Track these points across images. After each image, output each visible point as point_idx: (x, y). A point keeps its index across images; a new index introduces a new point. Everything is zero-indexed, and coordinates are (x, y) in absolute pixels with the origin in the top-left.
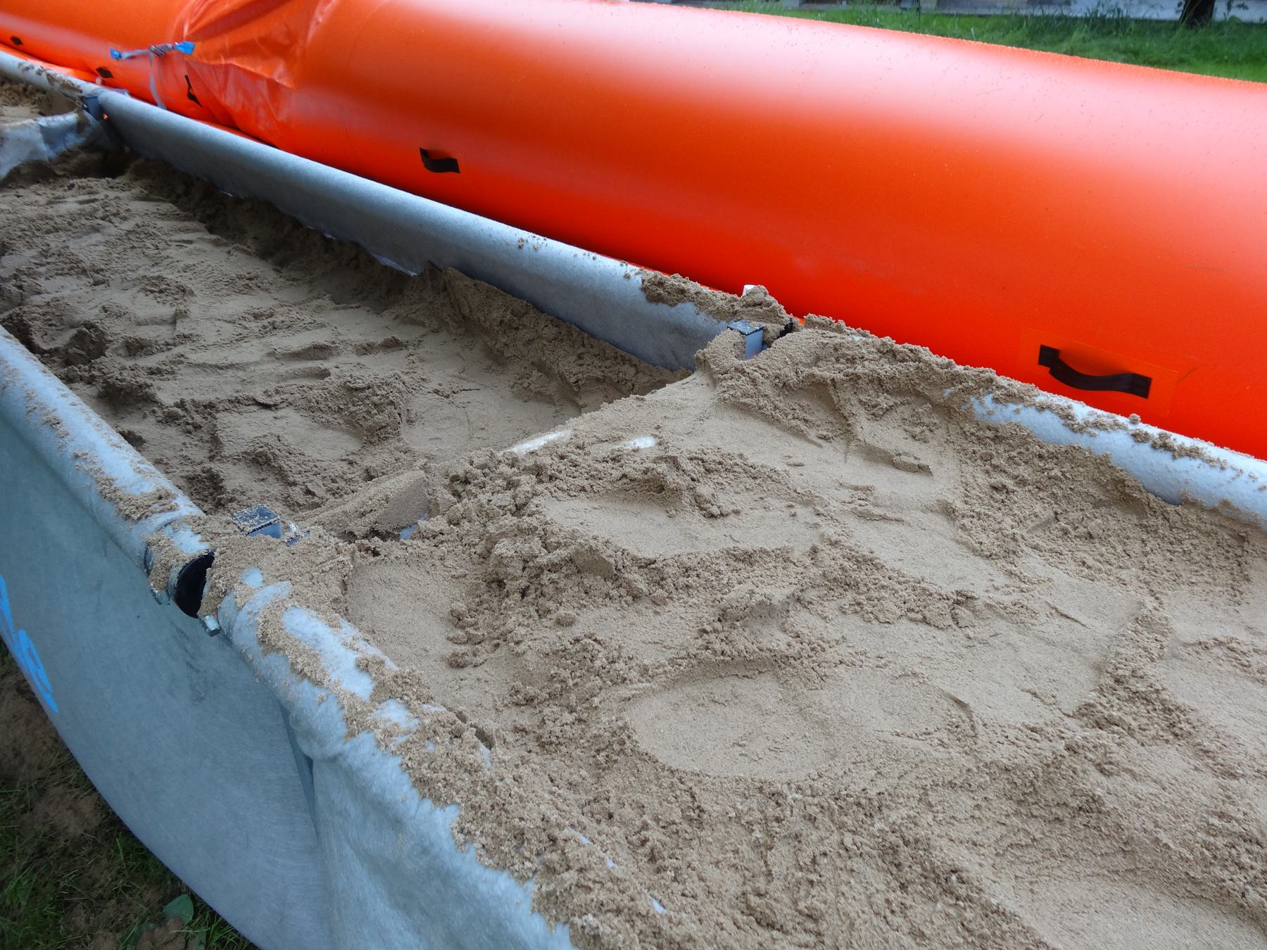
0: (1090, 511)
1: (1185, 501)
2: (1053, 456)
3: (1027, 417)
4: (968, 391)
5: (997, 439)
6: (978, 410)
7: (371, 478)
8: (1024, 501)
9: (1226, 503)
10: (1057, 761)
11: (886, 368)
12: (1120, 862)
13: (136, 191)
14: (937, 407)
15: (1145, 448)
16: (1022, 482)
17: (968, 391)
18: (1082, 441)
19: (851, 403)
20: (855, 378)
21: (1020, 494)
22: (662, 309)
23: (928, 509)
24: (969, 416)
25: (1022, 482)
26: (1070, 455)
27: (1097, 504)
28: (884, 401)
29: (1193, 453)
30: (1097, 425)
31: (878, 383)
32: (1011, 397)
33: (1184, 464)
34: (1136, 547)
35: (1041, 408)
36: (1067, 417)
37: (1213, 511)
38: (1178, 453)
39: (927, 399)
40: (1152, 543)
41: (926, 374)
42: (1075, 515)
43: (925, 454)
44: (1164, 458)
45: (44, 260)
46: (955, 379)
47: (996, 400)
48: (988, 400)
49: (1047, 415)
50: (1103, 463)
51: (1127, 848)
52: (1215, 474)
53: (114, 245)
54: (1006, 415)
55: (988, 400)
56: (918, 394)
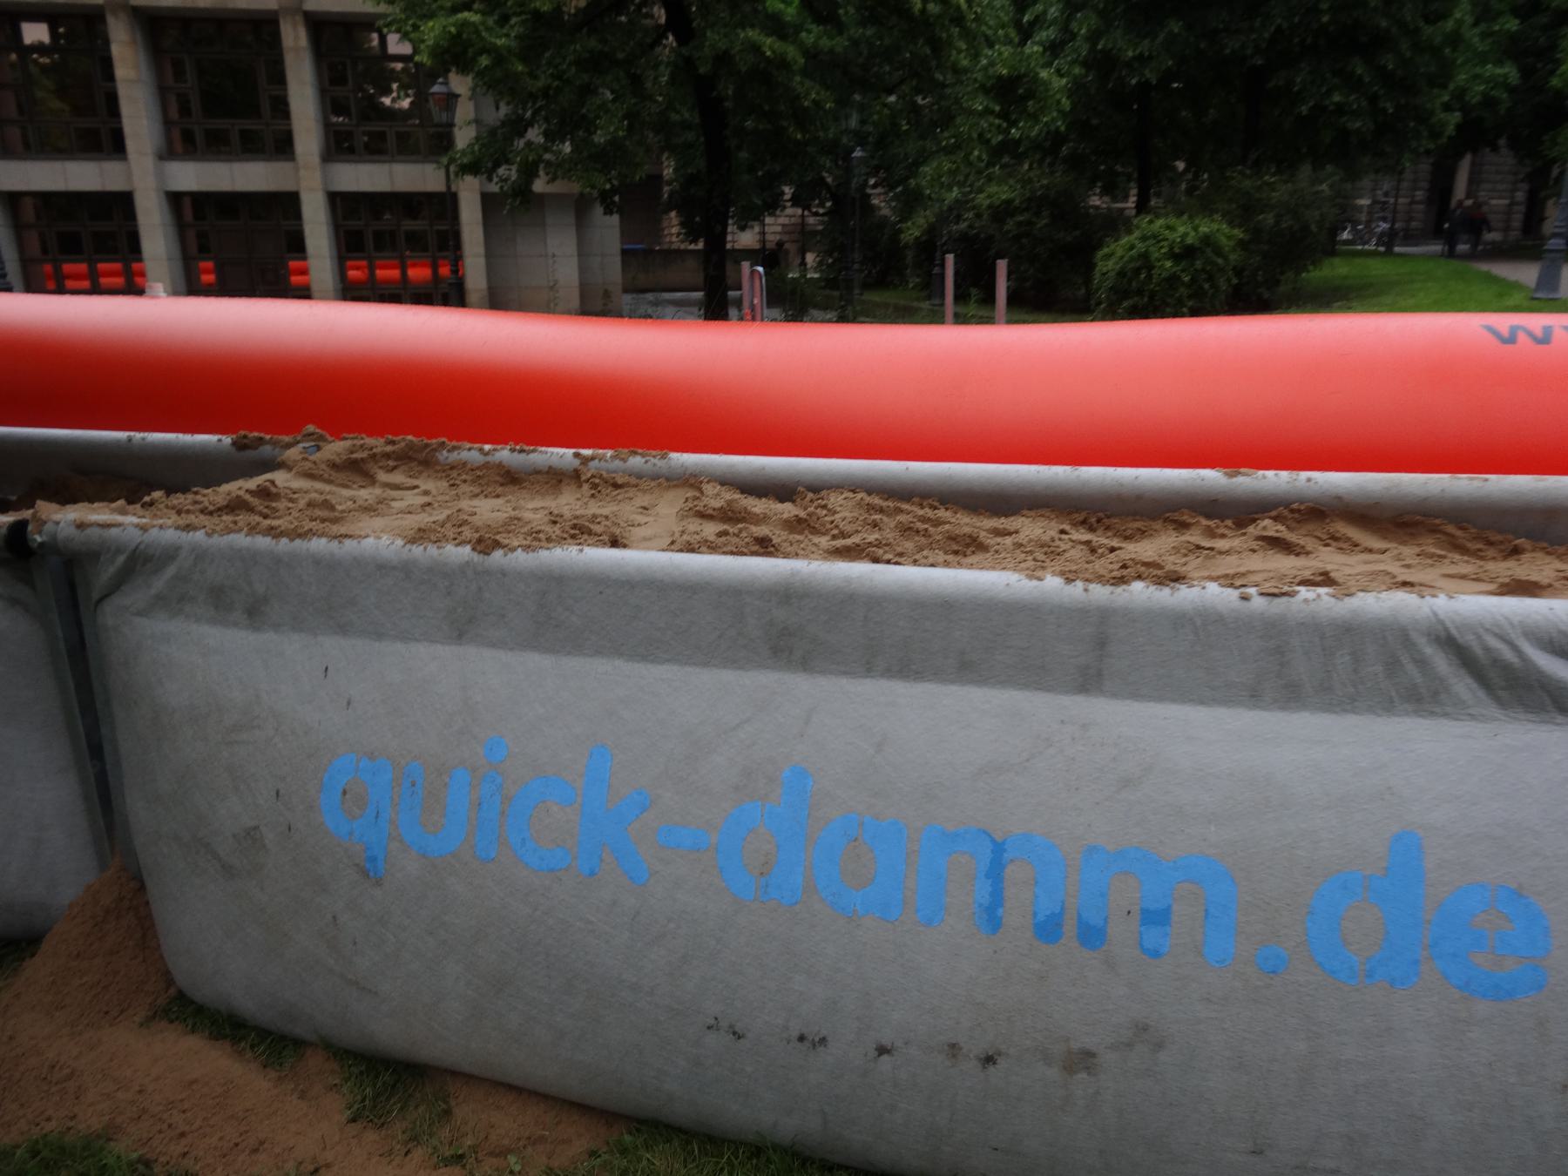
1: (537, 472)
5: (452, 468)
7: (953, 1046)
8: (465, 488)
11: (389, 448)
14: (421, 463)
17: (435, 450)
18: (489, 458)
19: (372, 468)
20: (374, 455)
22: (250, 454)
24: (437, 463)
26: (486, 466)
28: (391, 463)
31: (387, 456)
32: (454, 448)
33: (532, 456)
36: (481, 450)
38: (529, 452)
41: (410, 446)
43: (415, 482)
44: (523, 456)
45: (1405, 659)
46: (427, 446)
50: (500, 465)
53: (1129, 1045)
54: (454, 457)
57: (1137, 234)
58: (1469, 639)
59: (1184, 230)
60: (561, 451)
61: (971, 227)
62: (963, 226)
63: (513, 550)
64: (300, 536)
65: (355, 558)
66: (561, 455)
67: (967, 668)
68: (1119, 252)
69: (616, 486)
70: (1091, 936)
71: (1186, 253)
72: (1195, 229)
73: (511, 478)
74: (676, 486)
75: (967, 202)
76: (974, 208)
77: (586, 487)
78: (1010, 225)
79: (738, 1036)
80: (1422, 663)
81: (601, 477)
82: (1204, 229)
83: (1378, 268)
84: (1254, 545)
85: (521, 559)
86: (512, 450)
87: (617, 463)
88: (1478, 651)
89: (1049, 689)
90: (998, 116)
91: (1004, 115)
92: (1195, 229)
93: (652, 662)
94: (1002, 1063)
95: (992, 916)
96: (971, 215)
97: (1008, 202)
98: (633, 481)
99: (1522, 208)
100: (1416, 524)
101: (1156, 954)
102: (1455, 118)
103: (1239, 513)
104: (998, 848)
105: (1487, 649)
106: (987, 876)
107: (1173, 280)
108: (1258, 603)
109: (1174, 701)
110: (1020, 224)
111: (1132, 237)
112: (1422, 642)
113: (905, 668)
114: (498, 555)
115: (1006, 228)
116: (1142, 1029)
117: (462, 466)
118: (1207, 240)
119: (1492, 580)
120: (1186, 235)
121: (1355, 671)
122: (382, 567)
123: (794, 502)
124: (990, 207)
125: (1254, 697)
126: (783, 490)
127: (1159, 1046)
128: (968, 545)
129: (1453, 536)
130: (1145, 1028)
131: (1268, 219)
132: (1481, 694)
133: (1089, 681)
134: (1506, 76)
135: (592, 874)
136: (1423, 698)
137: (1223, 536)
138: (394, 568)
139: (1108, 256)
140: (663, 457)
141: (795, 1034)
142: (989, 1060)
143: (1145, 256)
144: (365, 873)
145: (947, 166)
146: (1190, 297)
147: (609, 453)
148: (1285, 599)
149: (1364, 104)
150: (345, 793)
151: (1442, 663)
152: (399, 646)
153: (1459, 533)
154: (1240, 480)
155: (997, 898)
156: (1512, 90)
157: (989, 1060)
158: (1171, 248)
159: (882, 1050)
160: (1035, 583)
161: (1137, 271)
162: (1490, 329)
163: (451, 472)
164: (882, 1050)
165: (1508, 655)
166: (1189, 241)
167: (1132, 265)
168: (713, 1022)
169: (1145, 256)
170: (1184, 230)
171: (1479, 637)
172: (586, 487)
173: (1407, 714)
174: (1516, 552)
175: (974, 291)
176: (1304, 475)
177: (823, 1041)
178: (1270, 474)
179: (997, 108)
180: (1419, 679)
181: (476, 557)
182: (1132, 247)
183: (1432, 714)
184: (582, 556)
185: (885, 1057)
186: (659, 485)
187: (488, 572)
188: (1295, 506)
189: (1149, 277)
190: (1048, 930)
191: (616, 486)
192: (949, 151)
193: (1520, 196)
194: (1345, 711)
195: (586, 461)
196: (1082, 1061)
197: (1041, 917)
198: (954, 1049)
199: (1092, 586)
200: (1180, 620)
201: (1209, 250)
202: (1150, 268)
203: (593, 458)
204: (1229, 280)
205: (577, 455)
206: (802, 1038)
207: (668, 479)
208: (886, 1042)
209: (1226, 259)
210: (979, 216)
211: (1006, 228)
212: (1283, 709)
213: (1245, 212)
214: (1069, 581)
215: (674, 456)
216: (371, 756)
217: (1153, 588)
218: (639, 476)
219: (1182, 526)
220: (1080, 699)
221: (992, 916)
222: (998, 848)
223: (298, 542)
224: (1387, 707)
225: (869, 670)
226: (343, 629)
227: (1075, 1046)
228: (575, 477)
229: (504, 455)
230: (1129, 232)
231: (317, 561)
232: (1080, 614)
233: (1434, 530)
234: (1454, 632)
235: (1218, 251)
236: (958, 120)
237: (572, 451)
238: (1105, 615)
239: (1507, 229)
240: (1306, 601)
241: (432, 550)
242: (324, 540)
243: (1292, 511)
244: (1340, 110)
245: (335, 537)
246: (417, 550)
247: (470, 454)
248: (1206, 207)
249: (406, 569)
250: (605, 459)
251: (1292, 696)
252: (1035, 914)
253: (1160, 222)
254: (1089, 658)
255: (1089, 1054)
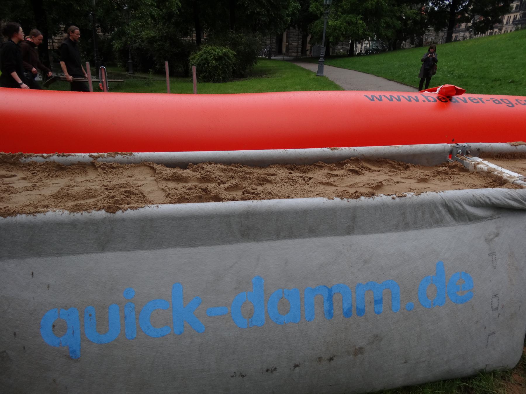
0: (55, 172)
1: (72, 164)
2: (43, 164)
3: (34, 159)
4: (17, 158)
5: (29, 165)
6: (22, 161)
9: (79, 162)
10: (59, 191)
12: (74, 199)
13: (254, 64)
14: (11, 164)
15: (61, 157)
16: (39, 171)
18: (48, 160)
21: (39, 173)
23: (20, 180)
24: (20, 163)
25: (39, 171)
26: (47, 163)
27: (56, 171)
29: (69, 155)
30: (49, 156)
32: (28, 156)
33: (69, 157)
34: (67, 175)
35: (36, 156)
36: (43, 156)
37: (78, 164)
38: (67, 156)
39: (8, 163)
40: (69, 173)
41: (5, 157)
42: (52, 174)
43: (13, 173)
44: (65, 158)
46: (13, 156)
47: (25, 158)
48: (23, 158)
49: (38, 157)
50: (54, 162)
51: (74, 197)
52: (75, 157)
53: (373, 342)
54: (29, 160)
55: (23, 158)
56: (5, 162)
57: (202, 51)
58: (450, 204)
59: (219, 51)
60: (83, 154)
61: (140, 45)
62: (137, 45)
63: (126, 210)
64: (9, 215)
65: (44, 222)
66: (84, 156)
67: (312, 232)
68: (197, 57)
69: (113, 168)
70: (361, 312)
71: (219, 59)
72: (221, 50)
73: (61, 168)
74: (139, 166)
75: (137, 36)
76: (140, 38)
77: (99, 169)
78: (155, 45)
79: (243, 376)
80: (439, 212)
81: (105, 165)
82: (224, 50)
83: (269, 64)
84: (349, 172)
85: (130, 213)
86: (58, 156)
87: (111, 158)
88: (452, 207)
89: (338, 235)
90: (155, 7)
91: (158, 7)
92: (221, 50)
93: (193, 246)
94: (335, 359)
95: (330, 314)
96: (139, 41)
97: (154, 37)
98: (119, 165)
99: (301, 46)
100: (382, 161)
101: (379, 313)
102: (289, 19)
103: (340, 162)
104: (330, 291)
105: (455, 206)
106: (327, 301)
107: (216, 67)
108: (397, 199)
109: (375, 233)
110: (159, 45)
111: (201, 52)
112: (439, 206)
113: (292, 234)
114: (119, 213)
115: (154, 46)
116: (376, 336)
117: (35, 164)
118: (225, 54)
119: (415, 179)
120: (219, 52)
121: (423, 217)
122: (60, 225)
123: (188, 169)
124: (147, 38)
125: (396, 228)
126: (184, 165)
127: (381, 340)
128: (263, 181)
129: (392, 164)
130: (377, 336)
131: (242, 48)
132: (452, 219)
133: (349, 231)
134: (297, 6)
135: (181, 333)
136: (439, 222)
137: (335, 170)
138: (67, 224)
139: (193, 59)
140: (131, 155)
141: (265, 370)
142: (331, 359)
143: (206, 59)
144: (70, 358)
145: (139, 24)
146: (222, 73)
147: (106, 154)
148: (404, 198)
149: (266, 12)
150: (54, 326)
151: (443, 211)
152: (73, 258)
153: (393, 163)
154: (336, 151)
155: (331, 307)
156: (299, 11)
157: (331, 359)
158: (214, 57)
159: (296, 366)
160: (332, 201)
161: (204, 64)
162: (366, 96)
163: (28, 167)
164: (296, 366)
165: (460, 207)
166: (220, 54)
167: (203, 62)
168: (233, 374)
169: (206, 59)
170: (219, 51)
171: (453, 203)
172: (99, 169)
173: (435, 227)
174: (407, 168)
175: (150, 70)
176: (353, 148)
177: (275, 369)
178: (343, 148)
179: (156, 4)
180: (438, 217)
181: (108, 214)
182: (202, 56)
183: (441, 226)
184: (159, 209)
185: (297, 368)
186: (132, 166)
187: (116, 221)
188: (352, 158)
189: (208, 66)
190: (347, 314)
191: (113, 168)
192: (140, 18)
193: (300, 42)
194: (420, 229)
195: (96, 158)
196: (360, 351)
197: (345, 310)
198: (320, 359)
199: (350, 200)
200: (377, 208)
201: (226, 58)
202: (208, 63)
203: (99, 157)
204: (233, 68)
205: (91, 156)
206: (267, 370)
207: (134, 164)
208: (297, 363)
209: (231, 61)
210: (143, 41)
211: (154, 46)
212: (404, 231)
213: (234, 45)
214: (342, 199)
215: (135, 153)
216: (66, 308)
217: (367, 198)
218: (122, 163)
219: (321, 167)
220: (348, 237)
221: (330, 314)
222: (330, 291)
223: (9, 218)
224: (430, 226)
225: (278, 238)
226: (39, 254)
227: (357, 347)
228: (93, 165)
229: (55, 157)
230: (200, 50)
231: (22, 226)
232: (347, 209)
233: (387, 163)
234: (447, 202)
235: (229, 58)
236: (141, 7)
237: (89, 154)
238: (355, 209)
239: (297, 52)
240: (410, 197)
241: (85, 214)
242: (24, 216)
243: (351, 160)
244: (258, 13)
245: (31, 213)
246: (78, 215)
247: (37, 158)
248: (224, 45)
249: (73, 224)
250: (104, 157)
251: (407, 227)
252: (343, 310)
253: (210, 47)
254: (349, 223)
255: (361, 348)
